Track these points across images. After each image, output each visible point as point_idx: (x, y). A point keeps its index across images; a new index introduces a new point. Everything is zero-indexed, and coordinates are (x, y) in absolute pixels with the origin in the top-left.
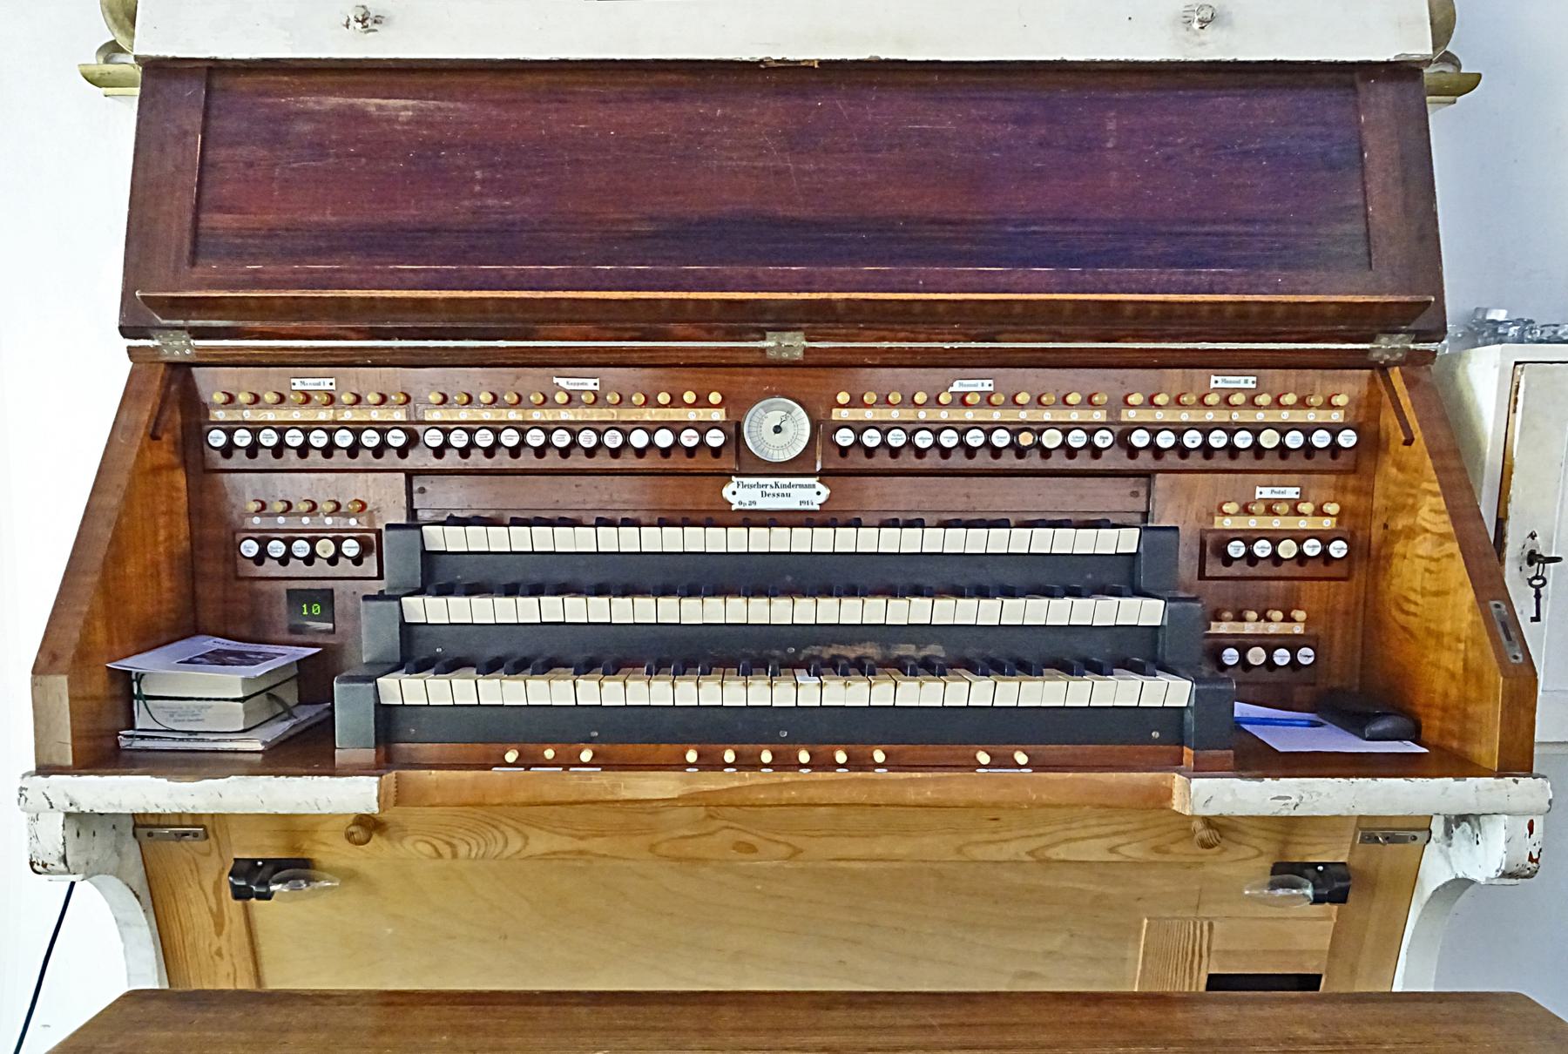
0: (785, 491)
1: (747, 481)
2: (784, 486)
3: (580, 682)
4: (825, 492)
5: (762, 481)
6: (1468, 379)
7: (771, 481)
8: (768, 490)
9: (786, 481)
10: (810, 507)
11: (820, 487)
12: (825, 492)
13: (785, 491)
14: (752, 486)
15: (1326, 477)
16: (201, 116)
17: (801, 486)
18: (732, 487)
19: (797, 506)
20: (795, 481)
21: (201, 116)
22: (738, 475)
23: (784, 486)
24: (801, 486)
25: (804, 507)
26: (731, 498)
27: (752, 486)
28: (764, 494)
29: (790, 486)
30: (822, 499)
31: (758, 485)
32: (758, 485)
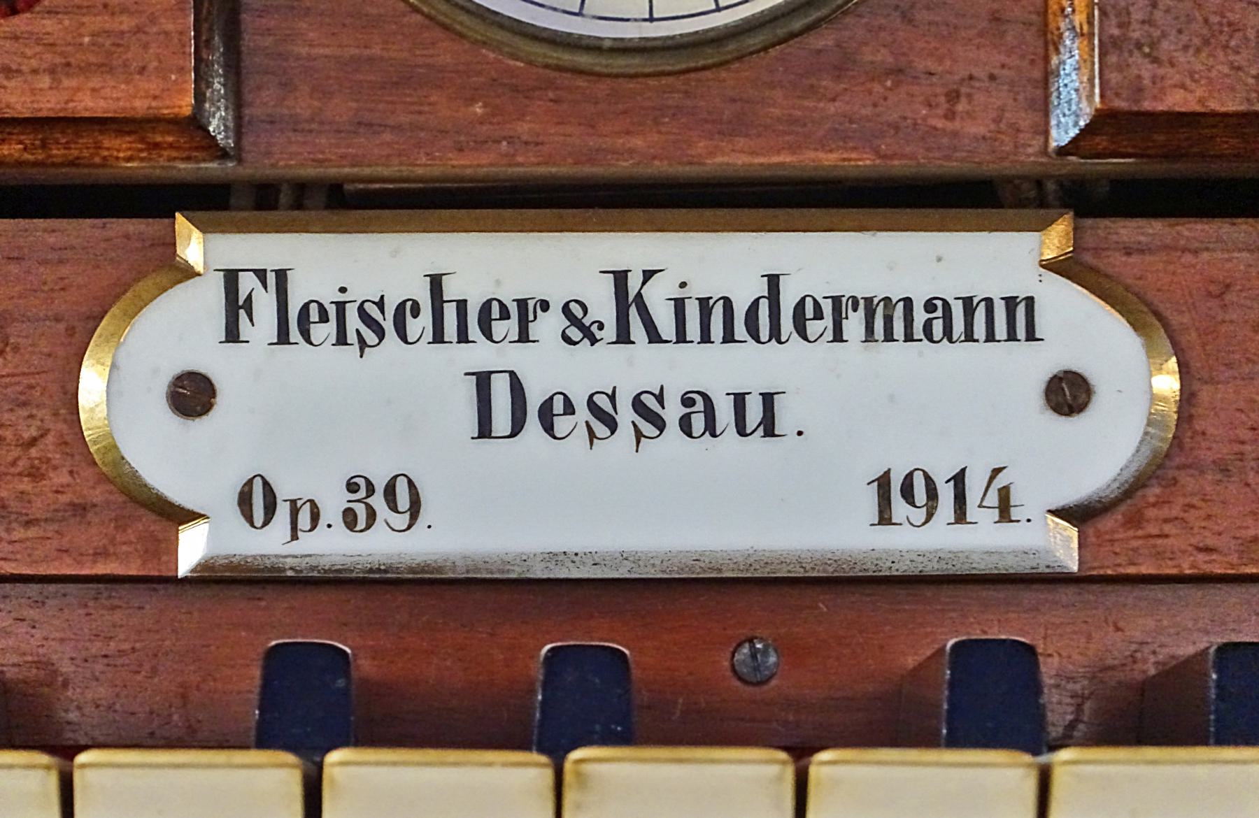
0: (723, 369)
1: (327, 263)
2: (711, 320)
3: (968, 520)
4: (1139, 384)
5: (486, 262)
6: (1015, 553)
7: (569, 263)
8: (549, 365)
9: (725, 262)
10: (982, 540)
11: (1082, 328)
12: (1139, 384)
13: (723, 369)
14: (374, 323)
15: (1152, 571)
16: (465, 301)
17: (887, 319)
18: (174, 328)
19: (845, 532)
20: (824, 261)
21: (465, 301)
22: (214, 202)
23: (711, 320)
24: (887, 319)
25: (921, 540)
26: (163, 455)
27: (374, 323)
28: (501, 410)
29: (770, 316)
30: (1103, 451)
31: (445, 315)
32: (445, 315)
